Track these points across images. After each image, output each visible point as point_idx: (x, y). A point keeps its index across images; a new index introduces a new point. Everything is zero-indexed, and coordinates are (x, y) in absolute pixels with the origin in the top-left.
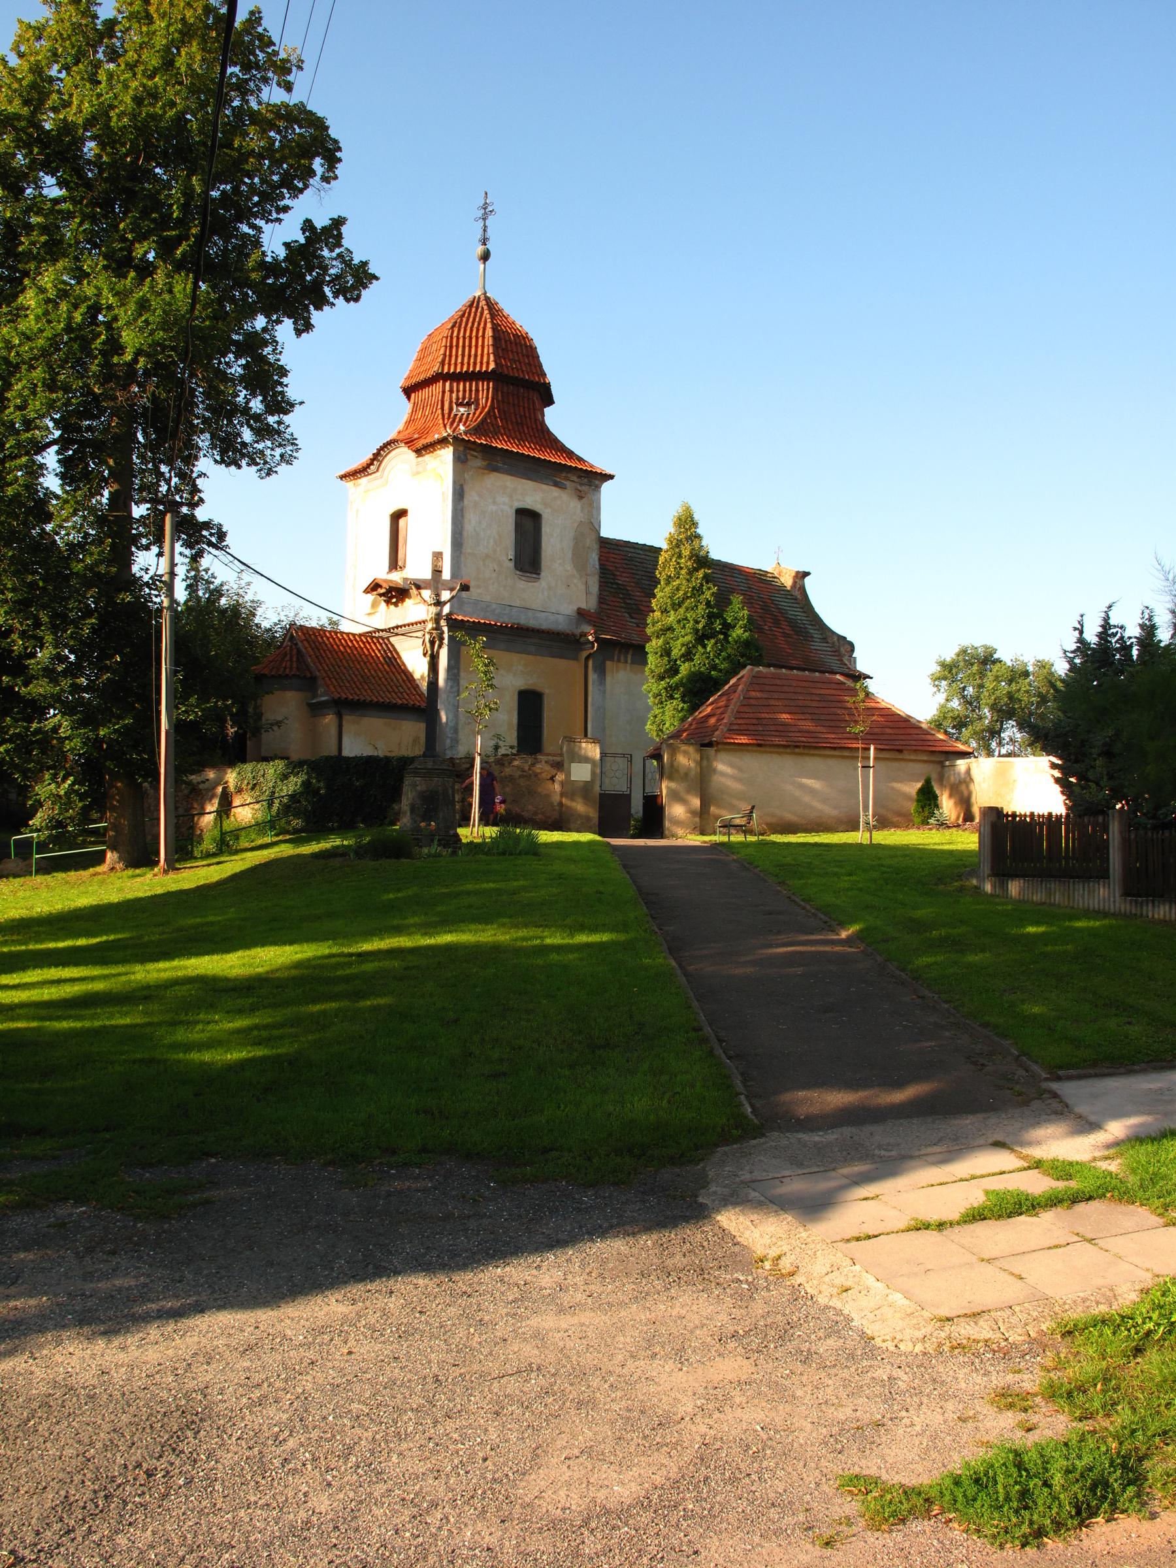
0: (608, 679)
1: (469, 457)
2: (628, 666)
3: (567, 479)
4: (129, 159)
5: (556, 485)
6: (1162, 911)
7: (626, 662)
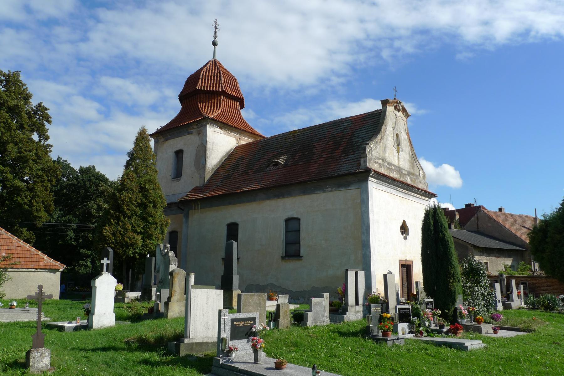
0: (190, 219)
1: (159, 139)
2: (199, 210)
3: (193, 129)
4: (60, 257)
5: (189, 133)
6: (1, 321)
7: (198, 209)
